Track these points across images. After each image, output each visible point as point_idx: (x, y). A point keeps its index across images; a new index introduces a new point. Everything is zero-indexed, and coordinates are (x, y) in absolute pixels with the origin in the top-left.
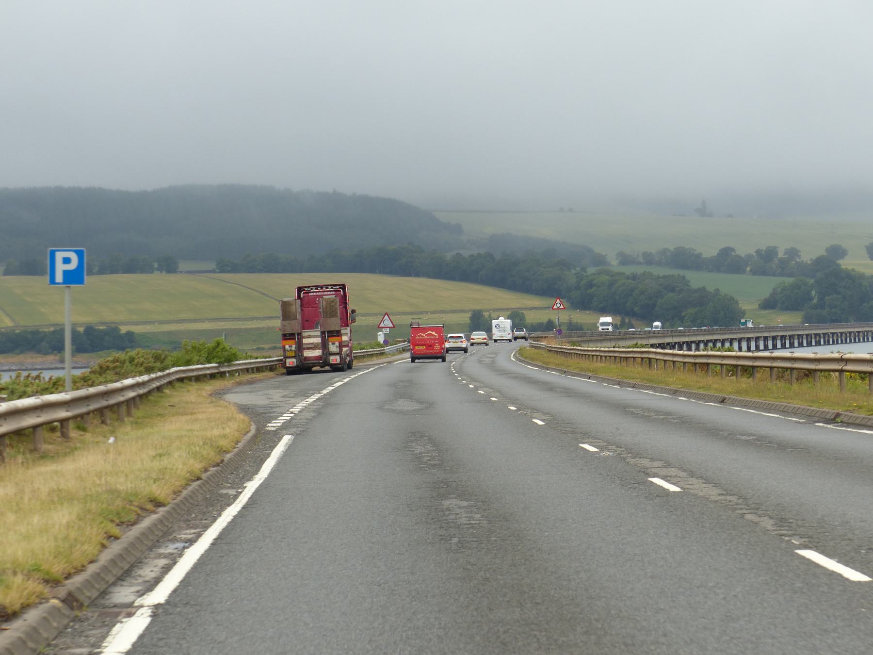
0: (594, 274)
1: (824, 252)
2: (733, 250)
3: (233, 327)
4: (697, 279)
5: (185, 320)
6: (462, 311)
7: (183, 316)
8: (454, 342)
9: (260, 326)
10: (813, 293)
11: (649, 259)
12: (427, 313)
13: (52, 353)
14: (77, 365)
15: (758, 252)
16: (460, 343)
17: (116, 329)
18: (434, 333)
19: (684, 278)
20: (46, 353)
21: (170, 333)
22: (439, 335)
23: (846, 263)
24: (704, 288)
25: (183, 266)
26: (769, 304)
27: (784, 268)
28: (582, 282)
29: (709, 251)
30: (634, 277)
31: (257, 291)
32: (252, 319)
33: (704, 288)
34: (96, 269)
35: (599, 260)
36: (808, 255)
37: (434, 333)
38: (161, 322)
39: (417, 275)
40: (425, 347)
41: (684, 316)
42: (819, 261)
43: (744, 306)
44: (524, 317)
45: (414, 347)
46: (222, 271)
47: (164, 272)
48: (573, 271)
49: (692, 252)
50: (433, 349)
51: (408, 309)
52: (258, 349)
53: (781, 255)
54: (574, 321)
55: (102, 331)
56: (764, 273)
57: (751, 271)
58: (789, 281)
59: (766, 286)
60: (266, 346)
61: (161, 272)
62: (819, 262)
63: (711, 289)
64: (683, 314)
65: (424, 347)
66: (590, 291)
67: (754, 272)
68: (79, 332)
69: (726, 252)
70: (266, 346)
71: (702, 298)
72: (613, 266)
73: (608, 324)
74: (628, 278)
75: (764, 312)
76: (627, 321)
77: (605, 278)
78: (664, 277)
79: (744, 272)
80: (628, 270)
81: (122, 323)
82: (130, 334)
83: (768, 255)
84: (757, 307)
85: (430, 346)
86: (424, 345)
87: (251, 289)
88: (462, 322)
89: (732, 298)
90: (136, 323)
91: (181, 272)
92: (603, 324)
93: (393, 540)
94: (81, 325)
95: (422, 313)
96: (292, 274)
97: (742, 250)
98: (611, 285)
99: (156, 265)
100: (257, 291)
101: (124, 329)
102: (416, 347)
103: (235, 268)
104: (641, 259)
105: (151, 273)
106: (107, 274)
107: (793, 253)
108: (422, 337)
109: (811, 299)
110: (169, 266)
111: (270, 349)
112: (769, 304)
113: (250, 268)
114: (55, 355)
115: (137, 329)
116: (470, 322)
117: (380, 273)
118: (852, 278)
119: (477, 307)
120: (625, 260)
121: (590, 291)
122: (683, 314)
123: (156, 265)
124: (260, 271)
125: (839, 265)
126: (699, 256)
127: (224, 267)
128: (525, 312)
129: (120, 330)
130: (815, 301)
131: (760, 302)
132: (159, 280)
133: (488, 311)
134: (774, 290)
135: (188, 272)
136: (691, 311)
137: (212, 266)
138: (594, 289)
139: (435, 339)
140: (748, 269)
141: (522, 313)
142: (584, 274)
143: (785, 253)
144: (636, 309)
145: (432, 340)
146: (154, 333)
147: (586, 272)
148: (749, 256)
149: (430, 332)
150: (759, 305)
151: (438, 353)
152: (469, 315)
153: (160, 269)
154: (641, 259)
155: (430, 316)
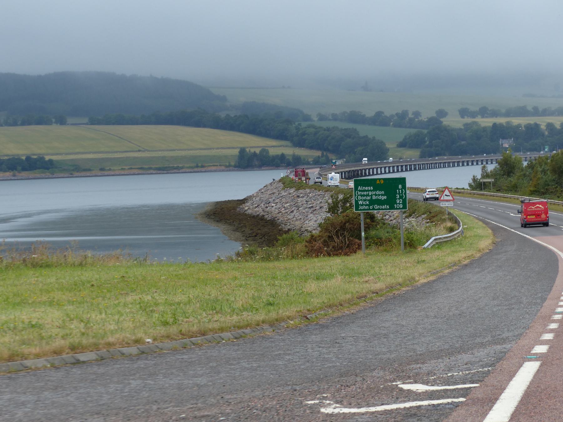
0: (306, 128)
1: (559, 123)
2: (383, 113)
3: (107, 157)
4: (364, 130)
5: (79, 153)
6: (233, 148)
7: (77, 150)
8: (432, 194)
9: (122, 156)
10: (426, 139)
11: (335, 118)
12: (214, 149)
13: (8, 171)
14: (22, 178)
15: (397, 114)
16: (435, 195)
17: (43, 158)
18: (541, 206)
19: (356, 130)
20: (5, 171)
21: (72, 160)
22: (545, 207)
23: (447, 121)
24: (367, 136)
25: (70, 120)
26: (402, 145)
27: (411, 124)
28: (299, 132)
29: (370, 113)
30: (328, 129)
31: (117, 136)
32: (116, 152)
33: (367, 136)
34: (20, 122)
35: (307, 118)
36: (424, 117)
37: (541, 206)
38: (67, 154)
39: (205, 126)
40: (534, 216)
41: (356, 151)
42: (431, 120)
43: (388, 146)
44: (269, 152)
45: (527, 217)
46: (92, 124)
47: (58, 124)
48: (294, 125)
49: (360, 114)
50: (540, 218)
51: (202, 147)
52: (122, 169)
53: (411, 116)
54: (296, 154)
55: (35, 159)
56: (400, 126)
57: (393, 125)
58: (413, 131)
59: (401, 134)
60: (127, 168)
61: (57, 124)
62: (431, 120)
63: (370, 136)
64: (355, 150)
65: (534, 217)
66: (304, 137)
67: (395, 126)
68: (22, 160)
69: (379, 114)
70: (127, 168)
71: (366, 142)
72: (314, 121)
73: (366, 161)
74: (325, 130)
75: (399, 149)
76: (325, 154)
77: (312, 130)
78: (345, 129)
79: (389, 125)
80: (325, 124)
81: (48, 154)
82: (51, 161)
83: (403, 116)
84: (396, 146)
85: (538, 215)
86: (534, 215)
87: (113, 135)
88: (234, 154)
89: (382, 142)
90: (52, 155)
91: (68, 124)
92: (364, 161)
93: (271, 299)
94: (23, 155)
95: (210, 149)
96: (132, 126)
97: (388, 112)
98: (316, 134)
99: (54, 120)
100: (117, 136)
101: (47, 158)
102: (528, 217)
103: (99, 123)
104: (330, 117)
105: (51, 125)
106: (26, 125)
107: (417, 114)
108: (532, 210)
109: (425, 142)
110: (61, 121)
111: (129, 169)
112: (402, 145)
113: (108, 122)
114: (10, 172)
115: (54, 158)
116: (238, 154)
117: (182, 125)
118: (447, 131)
119: (242, 146)
120: (322, 118)
121: (304, 137)
122: (355, 150)
123: (54, 120)
124: (114, 124)
125: (442, 122)
126: (364, 116)
127: (93, 122)
128: (268, 149)
129: (45, 158)
130: (428, 142)
131: (397, 143)
132: (56, 129)
133: (248, 148)
134: (405, 136)
135: (72, 124)
136: (360, 148)
137: (86, 120)
138: (306, 136)
139: (542, 211)
140: (391, 124)
141: (267, 149)
142: (300, 127)
143: (413, 114)
144: (330, 147)
145: (539, 211)
146: (64, 160)
147: (301, 126)
148: (392, 116)
149: (538, 205)
150: (397, 145)
151: (544, 220)
152: (238, 150)
153: (56, 123)
154: (330, 117)
155: (215, 151)
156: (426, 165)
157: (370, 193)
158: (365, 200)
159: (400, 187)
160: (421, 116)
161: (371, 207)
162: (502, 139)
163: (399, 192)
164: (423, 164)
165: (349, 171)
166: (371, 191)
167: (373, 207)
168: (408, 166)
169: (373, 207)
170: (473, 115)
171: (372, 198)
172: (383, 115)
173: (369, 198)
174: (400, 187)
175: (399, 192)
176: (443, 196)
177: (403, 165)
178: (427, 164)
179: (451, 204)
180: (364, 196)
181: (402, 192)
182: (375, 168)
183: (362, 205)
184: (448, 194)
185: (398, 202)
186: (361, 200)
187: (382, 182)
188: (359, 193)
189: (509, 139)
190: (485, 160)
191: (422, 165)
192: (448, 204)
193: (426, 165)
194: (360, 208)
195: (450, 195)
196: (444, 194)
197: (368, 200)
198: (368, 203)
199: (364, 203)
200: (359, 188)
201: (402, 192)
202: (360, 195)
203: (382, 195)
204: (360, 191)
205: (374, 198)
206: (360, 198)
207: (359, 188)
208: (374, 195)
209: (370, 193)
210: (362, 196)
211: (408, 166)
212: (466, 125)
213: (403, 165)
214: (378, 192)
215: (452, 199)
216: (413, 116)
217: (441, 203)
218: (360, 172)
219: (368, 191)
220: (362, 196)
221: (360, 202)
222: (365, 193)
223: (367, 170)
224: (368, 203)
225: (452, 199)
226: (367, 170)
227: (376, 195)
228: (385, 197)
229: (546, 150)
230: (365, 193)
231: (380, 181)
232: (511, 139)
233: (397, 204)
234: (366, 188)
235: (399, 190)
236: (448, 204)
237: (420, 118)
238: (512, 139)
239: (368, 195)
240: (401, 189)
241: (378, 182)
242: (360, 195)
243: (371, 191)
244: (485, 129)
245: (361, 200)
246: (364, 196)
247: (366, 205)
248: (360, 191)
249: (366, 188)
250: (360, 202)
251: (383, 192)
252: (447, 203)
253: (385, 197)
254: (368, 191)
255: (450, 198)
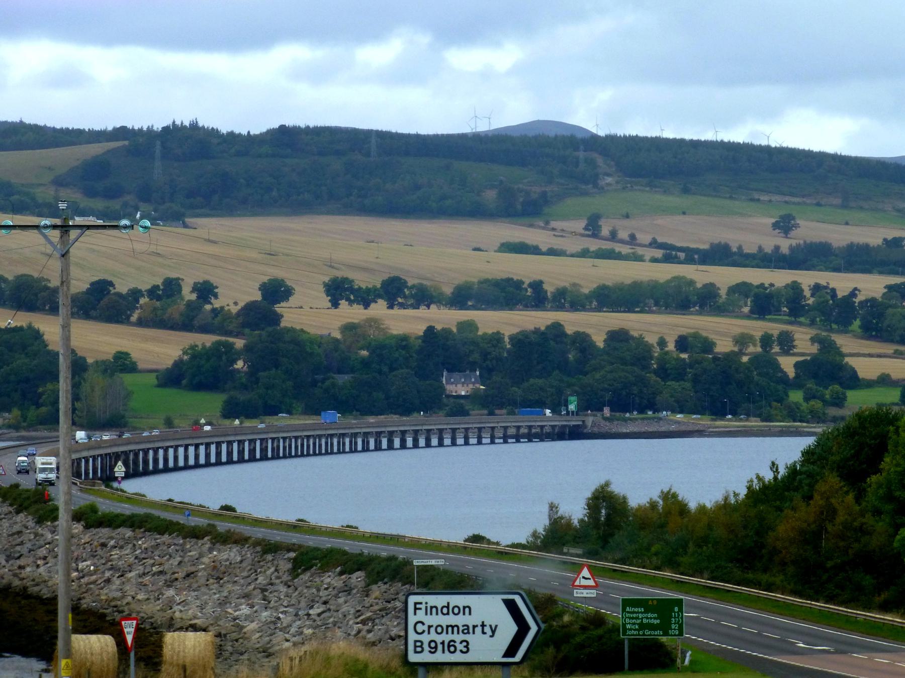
2: (111, 284)
58: (207, 340)
156: (293, 440)
157: (640, 616)
158: (634, 624)
159: (676, 609)
160: (216, 296)
161: (641, 633)
162: (449, 371)
163: (675, 615)
164: (284, 439)
165: (106, 455)
166: (641, 613)
167: (644, 632)
168: (258, 443)
169: (644, 632)
170: (365, 298)
171: (642, 621)
172: (113, 291)
173: (639, 621)
174: (676, 609)
175: (675, 615)
176: (578, 579)
177: (245, 441)
178: (296, 438)
179: (592, 593)
180: (633, 618)
181: (679, 615)
182: (172, 447)
183: (631, 629)
184: (588, 575)
185: (673, 627)
186: (629, 623)
187: (655, 603)
188: (628, 615)
189: (468, 372)
190: (435, 431)
191: (281, 441)
192: (587, 593)
193: (293, 440)
194: (628, 632)
195: (591, 577)
196: (581, 576)
197: (638, 624)
198: (637, 627)
199: (633, 627)
200: (628, 609)
201: (679, 615)
202: (629, 618)
203: (655, 618)
204: (628, 612)
205: (645, 621)
206: (628, 621)
207: (628, 609)
208: (645, 618)
209: (640, 616)
210: (630, 618)
211: (258, 443)
212: (349, 328)
213: (245, 441)
214: (649, 615)
215: (594, 584)
216: (194, 297)
217: (575, 591)
218: (131, 457)
219: (638, 612)
220: (630, 618)
221: (628, 626)
222: (634, 615)
223: (151, 452)
224: (637, 627)
225: (594, 584)
226: (151, 452)
227: (647, 618)
228: (658, 621)
229: (572, 407)
230: (634, 615)
231: (652, 602)
232: (475, 371)
233: (671, 629)
234: (636, 610)
235: (675, 612)
236: (587, 593)
237: (217, 304)
238: (478, 373)
239: (637, 618)
240: (678, 612)
241: (650, 603)
242: (629, 618)
243: (641, 613)
244: (403, 342)
245: (629, 623)
246: (633, 618)
247: (635, 630)
248: (628, 612)
249: (636, 610)
250: (628, 626)
251: (656, 615)
252: (585, 591)
253: (658, 621)
254: (638, 612)
255: (591, 583)
